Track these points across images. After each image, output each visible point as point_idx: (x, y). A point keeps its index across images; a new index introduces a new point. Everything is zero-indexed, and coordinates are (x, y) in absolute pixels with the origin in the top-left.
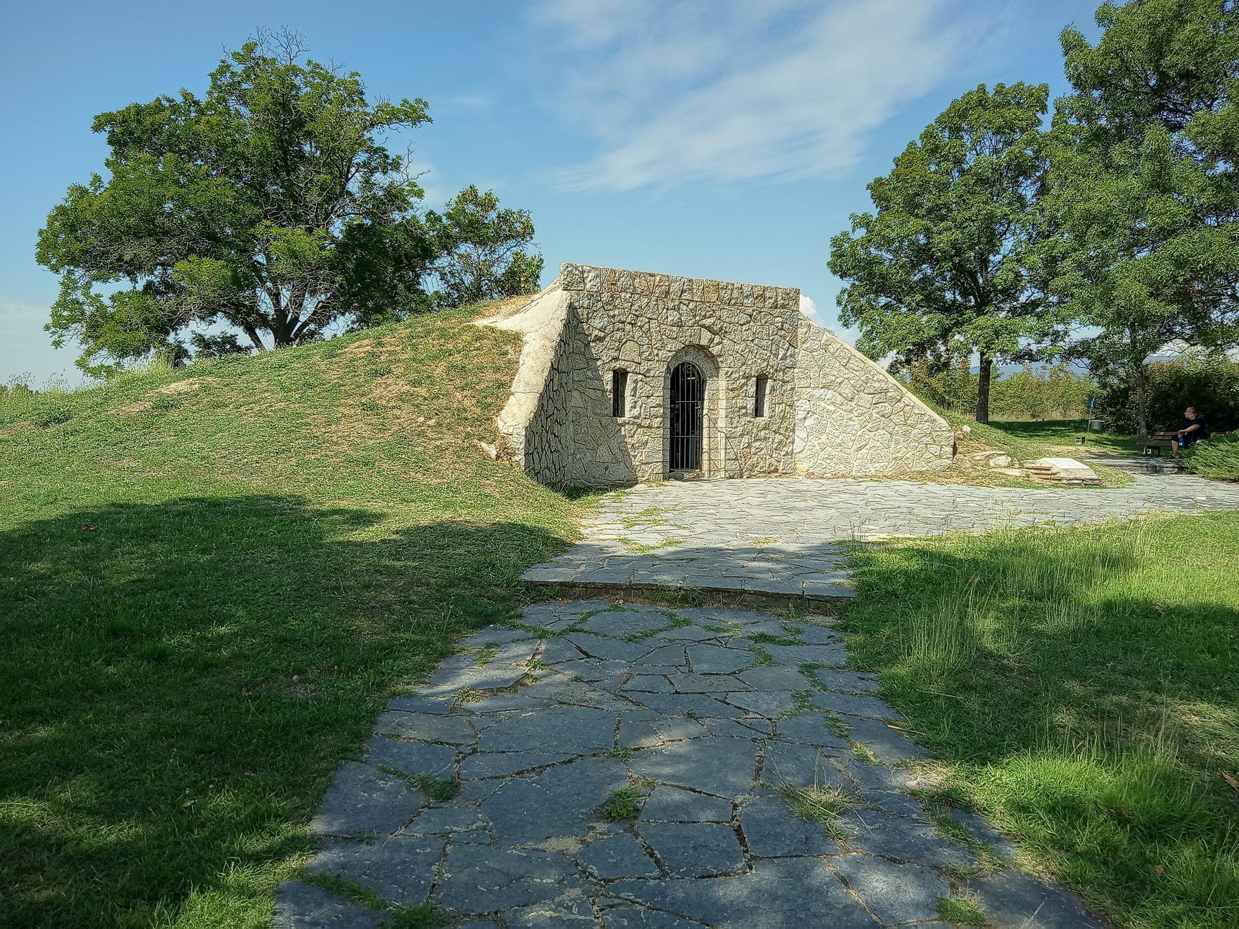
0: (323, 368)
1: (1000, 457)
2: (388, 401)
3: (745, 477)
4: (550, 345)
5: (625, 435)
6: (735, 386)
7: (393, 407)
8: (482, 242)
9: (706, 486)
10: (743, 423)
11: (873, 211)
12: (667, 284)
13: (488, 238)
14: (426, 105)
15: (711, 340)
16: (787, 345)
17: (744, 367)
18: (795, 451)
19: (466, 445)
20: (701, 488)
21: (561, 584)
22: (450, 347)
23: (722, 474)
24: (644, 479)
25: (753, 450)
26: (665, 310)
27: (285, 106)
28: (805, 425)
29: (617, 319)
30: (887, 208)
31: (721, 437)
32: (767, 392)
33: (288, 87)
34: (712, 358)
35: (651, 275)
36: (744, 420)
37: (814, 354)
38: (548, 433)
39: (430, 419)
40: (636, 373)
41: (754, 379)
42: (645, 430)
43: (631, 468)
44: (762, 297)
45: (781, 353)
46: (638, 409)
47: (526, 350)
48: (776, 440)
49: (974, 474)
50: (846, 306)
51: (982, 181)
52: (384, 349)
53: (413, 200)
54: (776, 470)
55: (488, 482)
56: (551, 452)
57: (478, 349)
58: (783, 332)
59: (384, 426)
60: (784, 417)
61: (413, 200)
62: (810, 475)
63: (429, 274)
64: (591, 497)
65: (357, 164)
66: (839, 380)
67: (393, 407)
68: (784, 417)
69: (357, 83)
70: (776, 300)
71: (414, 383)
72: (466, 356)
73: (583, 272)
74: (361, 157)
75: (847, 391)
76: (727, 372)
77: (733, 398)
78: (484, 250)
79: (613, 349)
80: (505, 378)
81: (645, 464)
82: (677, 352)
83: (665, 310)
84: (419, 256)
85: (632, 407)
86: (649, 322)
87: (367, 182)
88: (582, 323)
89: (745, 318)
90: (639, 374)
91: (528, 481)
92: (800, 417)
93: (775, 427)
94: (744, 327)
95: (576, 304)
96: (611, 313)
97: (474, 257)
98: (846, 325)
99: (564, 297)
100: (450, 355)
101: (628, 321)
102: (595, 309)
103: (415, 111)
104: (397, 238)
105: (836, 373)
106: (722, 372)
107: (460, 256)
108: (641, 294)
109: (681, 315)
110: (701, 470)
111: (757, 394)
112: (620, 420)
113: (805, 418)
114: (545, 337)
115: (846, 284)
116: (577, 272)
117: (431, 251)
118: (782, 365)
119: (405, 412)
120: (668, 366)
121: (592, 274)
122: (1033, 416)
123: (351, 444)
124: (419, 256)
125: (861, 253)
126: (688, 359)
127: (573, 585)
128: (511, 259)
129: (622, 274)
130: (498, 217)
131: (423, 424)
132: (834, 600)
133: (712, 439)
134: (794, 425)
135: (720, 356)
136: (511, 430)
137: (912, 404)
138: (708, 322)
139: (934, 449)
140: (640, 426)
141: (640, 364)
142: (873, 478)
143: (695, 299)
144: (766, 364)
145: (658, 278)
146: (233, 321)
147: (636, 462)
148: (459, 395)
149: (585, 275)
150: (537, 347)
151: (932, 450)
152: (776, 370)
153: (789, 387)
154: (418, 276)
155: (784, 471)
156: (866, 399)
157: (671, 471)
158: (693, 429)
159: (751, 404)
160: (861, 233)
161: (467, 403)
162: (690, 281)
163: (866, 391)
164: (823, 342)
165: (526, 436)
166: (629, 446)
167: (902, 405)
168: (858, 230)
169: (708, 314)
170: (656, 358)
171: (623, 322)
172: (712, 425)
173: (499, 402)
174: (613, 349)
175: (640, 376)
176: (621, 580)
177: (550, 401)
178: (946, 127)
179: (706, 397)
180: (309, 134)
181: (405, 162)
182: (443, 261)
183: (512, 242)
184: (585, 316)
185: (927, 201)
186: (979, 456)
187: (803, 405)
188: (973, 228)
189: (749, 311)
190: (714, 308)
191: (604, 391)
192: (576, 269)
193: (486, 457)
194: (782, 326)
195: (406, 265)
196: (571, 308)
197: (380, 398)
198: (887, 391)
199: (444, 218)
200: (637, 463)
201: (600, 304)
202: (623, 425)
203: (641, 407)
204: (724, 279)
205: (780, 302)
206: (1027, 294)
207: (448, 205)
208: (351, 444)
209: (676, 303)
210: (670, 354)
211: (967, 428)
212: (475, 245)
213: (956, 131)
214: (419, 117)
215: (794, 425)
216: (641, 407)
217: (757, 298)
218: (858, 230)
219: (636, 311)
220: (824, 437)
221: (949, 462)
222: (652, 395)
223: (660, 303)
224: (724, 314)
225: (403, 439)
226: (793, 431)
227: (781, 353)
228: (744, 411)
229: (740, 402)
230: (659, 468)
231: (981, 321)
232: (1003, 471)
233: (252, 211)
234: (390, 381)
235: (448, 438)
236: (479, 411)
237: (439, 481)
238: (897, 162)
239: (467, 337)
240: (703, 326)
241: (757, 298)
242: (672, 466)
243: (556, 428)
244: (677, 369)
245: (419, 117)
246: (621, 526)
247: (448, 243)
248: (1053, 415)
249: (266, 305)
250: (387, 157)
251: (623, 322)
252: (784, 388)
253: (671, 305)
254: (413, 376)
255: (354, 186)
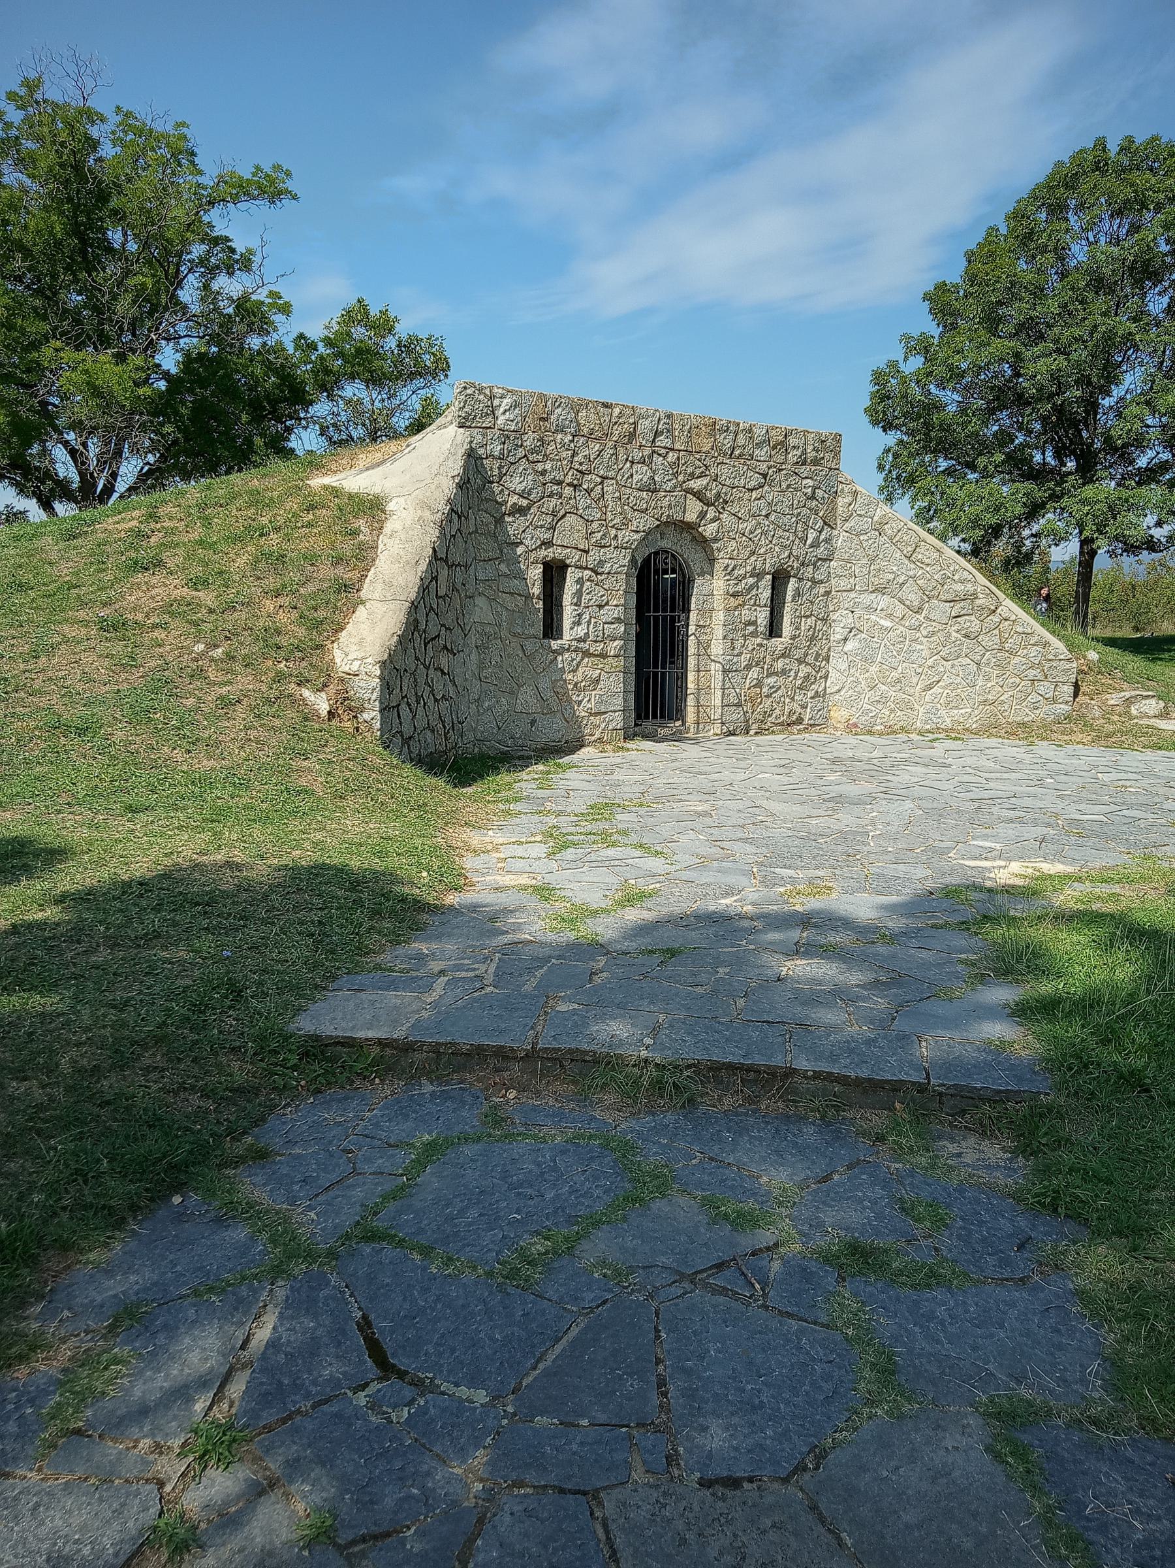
0: (54, 556)
1: (1147, 702)
2: (147, 616)
3: (752, 732)
4: (431, 518)
5: (562, 670)
6: (739, 588)
7: (155, 626)
8: (374, 380)
9: (690, 751)
10: (750, 648)
11: (933, 329)
12: (631, 421)
13: (384, 374)
14: (288, 174)
15: (702, 515)
16: (820, 523)
17: (753, 559)
18: (828, 691)
19: (274, 693)
20: (684, 755)
21: (380, 1042)
22: (265, 520)
23: (717, 728)
24: (593, 738)
25: (765, 689)
26: (628, 464)
27: (78, 168)
28: (846, 649)
29: (549, 477)
30: (954, 327)
31: (715, 670)
32: (789, 598)
33: (80, 141)
34: (703, 542)
35: (606, 405)
36: (753, 642)
37: (861, 538)
38: (428, 668)
39: (216, 646)
40: (581, 567)
41: (769, 577)
42: (596, 660)
43: (573, 721)
44: (782, 447)
45: (812, 535)
46: (584, 626)
47: (389, 527)
48: (801, 674)
49: (1109, 728)
50: (890, 472)
51: (1099, 284)
52: (158, 526)
53: (278, 318)
54: (800, 721)
55: (306, 763)
56: (436, 700)
57: (309, 525)
58: (815, 503)
59: (133, 659)
60: (813, 639)
61: (278, 318)
62: (851, 728)
63: (306, 428)
64: (504, 777)
65: (189, 261)
66: (901, 580)
67: (155, 626)
68: (813, 639)
69: (184, 138)
70: (804, 452)
71: (197, 583)
72: (287, 538)
73: (492, 398)
74: (198, 250)
75: (912, 596)
76: (728, 566)
77: (737, 607)
78: (379, 393)
79: (542, 527)
80: (350, 575)
81: (596, 714)
82: (648, 533)
83: (628, 464)
84: (286, 400)
85: (574, 623)
86: (602, 483)
87: (206, 287)
88: (492, 482)
89: (756, 479)
90: (586, 568)
91: (381, 758)
92: (838, 637)
93: (798, 654)
94: (754, 495)
95: (481, 451)
96: (540, 467)
97: (367, 401)
98: (890, 499)
99: (459, 438)
100: (261, 535)
101: (567, 481)
102: (512, 459)
103: (272, 183)
104: (253, 372)
105: (895, 569)
106: (719, 567)
107: (348, 402)
108: (589, 437)
109: (654, 472)
110: (684, 723)
111: (772, 601)
112: (555, 644)
113: (845, 640)
114: (424, 505)
115: (891, 439)
116: (481, 397)
117: (304, 391)
118: (812, 554)
119: (173, 636)
120: (633, 556)
121: (507, 401)
122: (1137, 629)
123: (68, 694)
124: (286, 400)
125: (916, 392)
126: (666, 544)
127: (406, 1047)
128: (418, 407)
129: (557, 402)
130: (399, 346)
131: (202, 655)
132: (998, 1098)
133: (702, 674)
134: (829, 650)
135: (716, 540)
136: (355, 666)
137: (1013, 617)
138: (696, 484)
139: (1044, 688)
140: (587, 654)
141: (587, 552)
142: (952, 734)
143: (677, 446)
144: (787, 553)
145: (617, 411)
146: (21, 491)
147: (581, 712)
148: (270, 605)
149: (496, 402)
150: (408, 522)
151: (1041, 690)
152: (803, 564)
153: (822, 591)
154: (289, 430)
155: (812, 722)
156: (940, 610)
157: (636, 725)
158: (672, 655)
159: (763, 617)
160: (916, 363)
161: (283, 617)
162: (670, 416)
163: (942, 597)
164: (876, 518)
165: (382, 678)
166: (570, 687)
167: (996, 619)
168: (911, 358)
169: (698, 471)
170: (614, 543)
171: (560, 483)
172: (702, 652)
173: (338, 618)
174: (542, 527)
175: (586, 572)
176: (518, 1038)
177: (432, 615)
178: (1043, 204)
179: (693, 606)
180: (118, 215)
181: (257, 259)
182: (321, 408)
183: (418, 382)
184: (496, 472)
185: (1016, 312)
186: (1114, 699)
187: (842, 621)
188: (1080, 354)
189: (763, 467)
190: (707, 462)
191: (528, 597)
192: (481, 391)
193: (309, 716)
194: (814, 493)
195: (270, 413)
196: (471, 455)
197: (135, 609)
198: (975, 596)
199: (321, 345)
200: (583, 714)
201: (521, 452)
202: (561, 651)
203: (589, 623)
204: (723, 416)
205: (811, 454)
206: (1151, 453)
207: (327, 327)
208: (68, 694)
209: (647, 452)
210: (636, 536)
211: (1093, 655)
212: (367, 387)
213: (1057, 209)
214: (280, 193)
215: (829, 650)
216: (589, 623)
217: (774, 448)
218: (911, 358)
219: (581, 464)
220: (874, 669)
221: (1067, 708)
222: (607, 604)
223: (621, 451)
224: (725, 471)
225: (163, 685)
226: (827, 659)
227: (812, 535)
228: (751, 628)
229: (746, 615)
230: (617, 721)
231: (1089, 491)
232: (1152, 722)
233: (36, 328)
234: (154, 580)
235: (245, 681)
236: (301, 632)
237: (213, 763)
238: (970, 257)
239: (293, 505)
240: (689, 491)
241: (774, 448)
242: (638, 717)
243: (444, 660)
244: (647, 561)
245: (280, 193)
246: (539, 850)
247: (327, 383)
248: (1164, 628)
249: (65, 468)
250: (233, 251)
251: (560, 483)
252: (815, 591)
253: (638, 455)
254: (197, 570)
255: (189, 293)
